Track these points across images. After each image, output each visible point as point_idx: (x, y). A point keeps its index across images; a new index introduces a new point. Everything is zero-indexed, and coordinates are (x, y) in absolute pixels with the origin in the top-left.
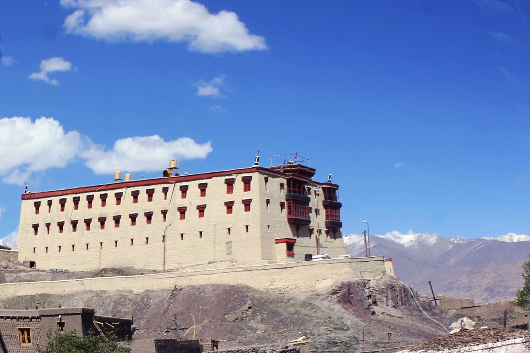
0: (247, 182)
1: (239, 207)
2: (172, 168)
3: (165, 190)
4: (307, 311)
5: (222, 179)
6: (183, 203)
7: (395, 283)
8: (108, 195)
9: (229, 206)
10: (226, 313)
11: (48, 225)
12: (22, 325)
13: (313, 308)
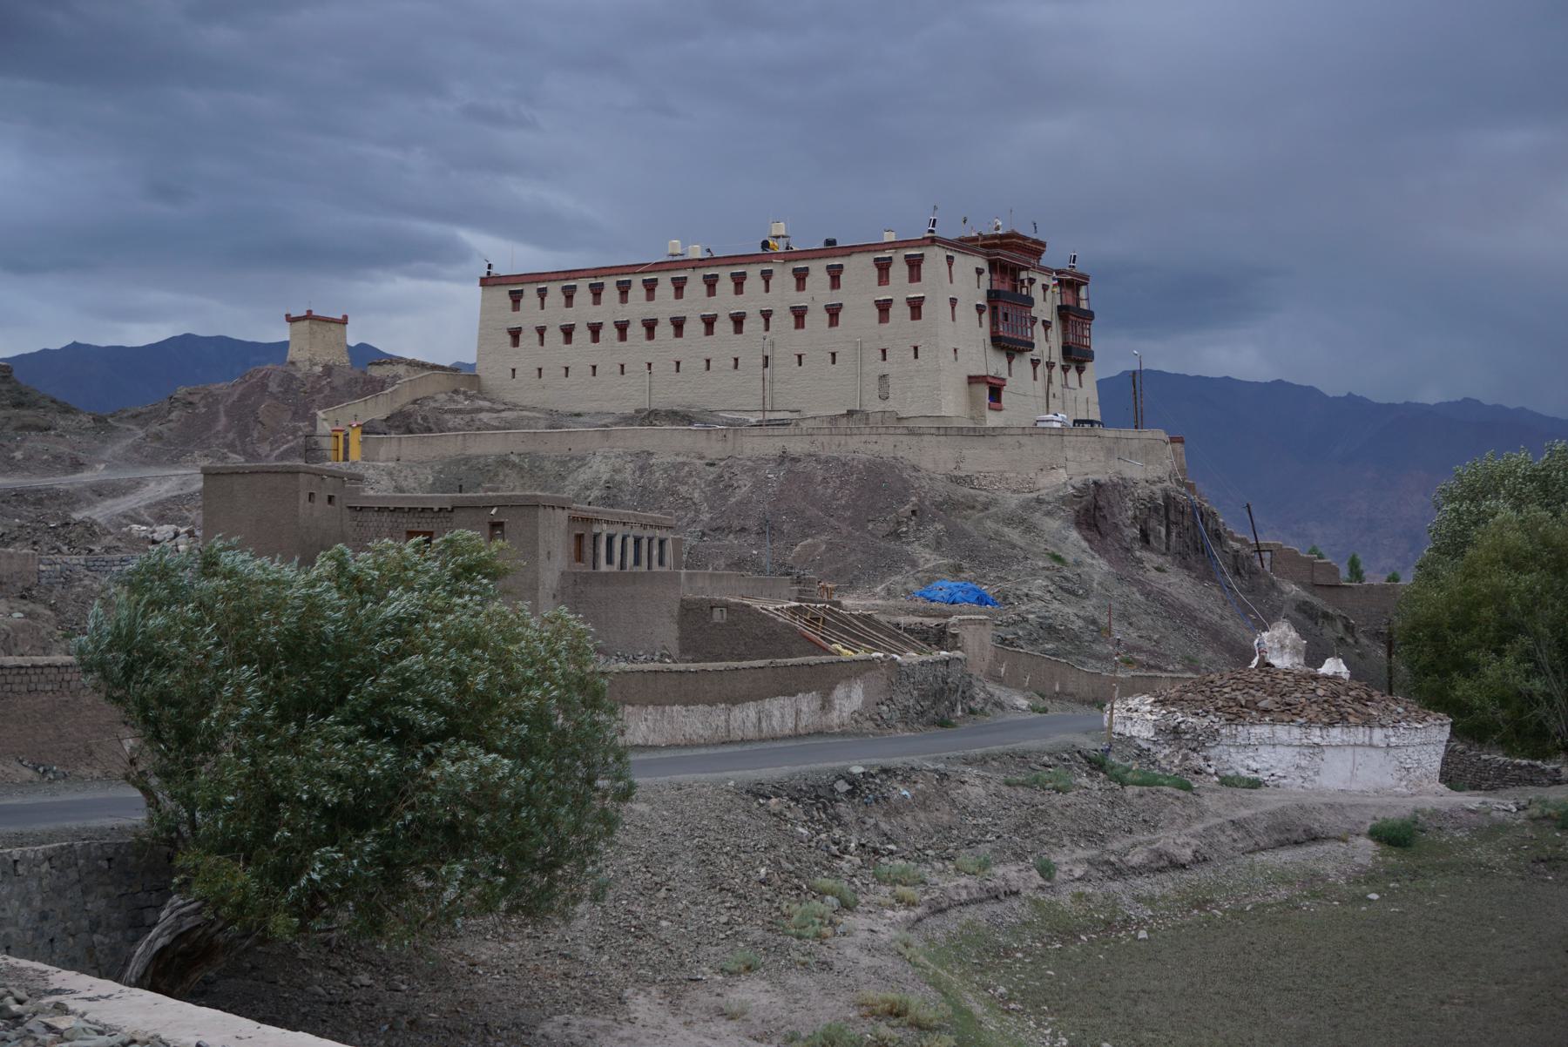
0: (914, 264)
1: (900, 311)
2: (778, 237)
3: (767, 276)
4: (1014, 534)
5: (868, 259)
6: (801, 299)
7: (1184, 495)
8: (605, 286)
9: (884, 307)
10: (870, 518)
11: (541, 331)
12: (416, 525)
13: (1028, 530)
